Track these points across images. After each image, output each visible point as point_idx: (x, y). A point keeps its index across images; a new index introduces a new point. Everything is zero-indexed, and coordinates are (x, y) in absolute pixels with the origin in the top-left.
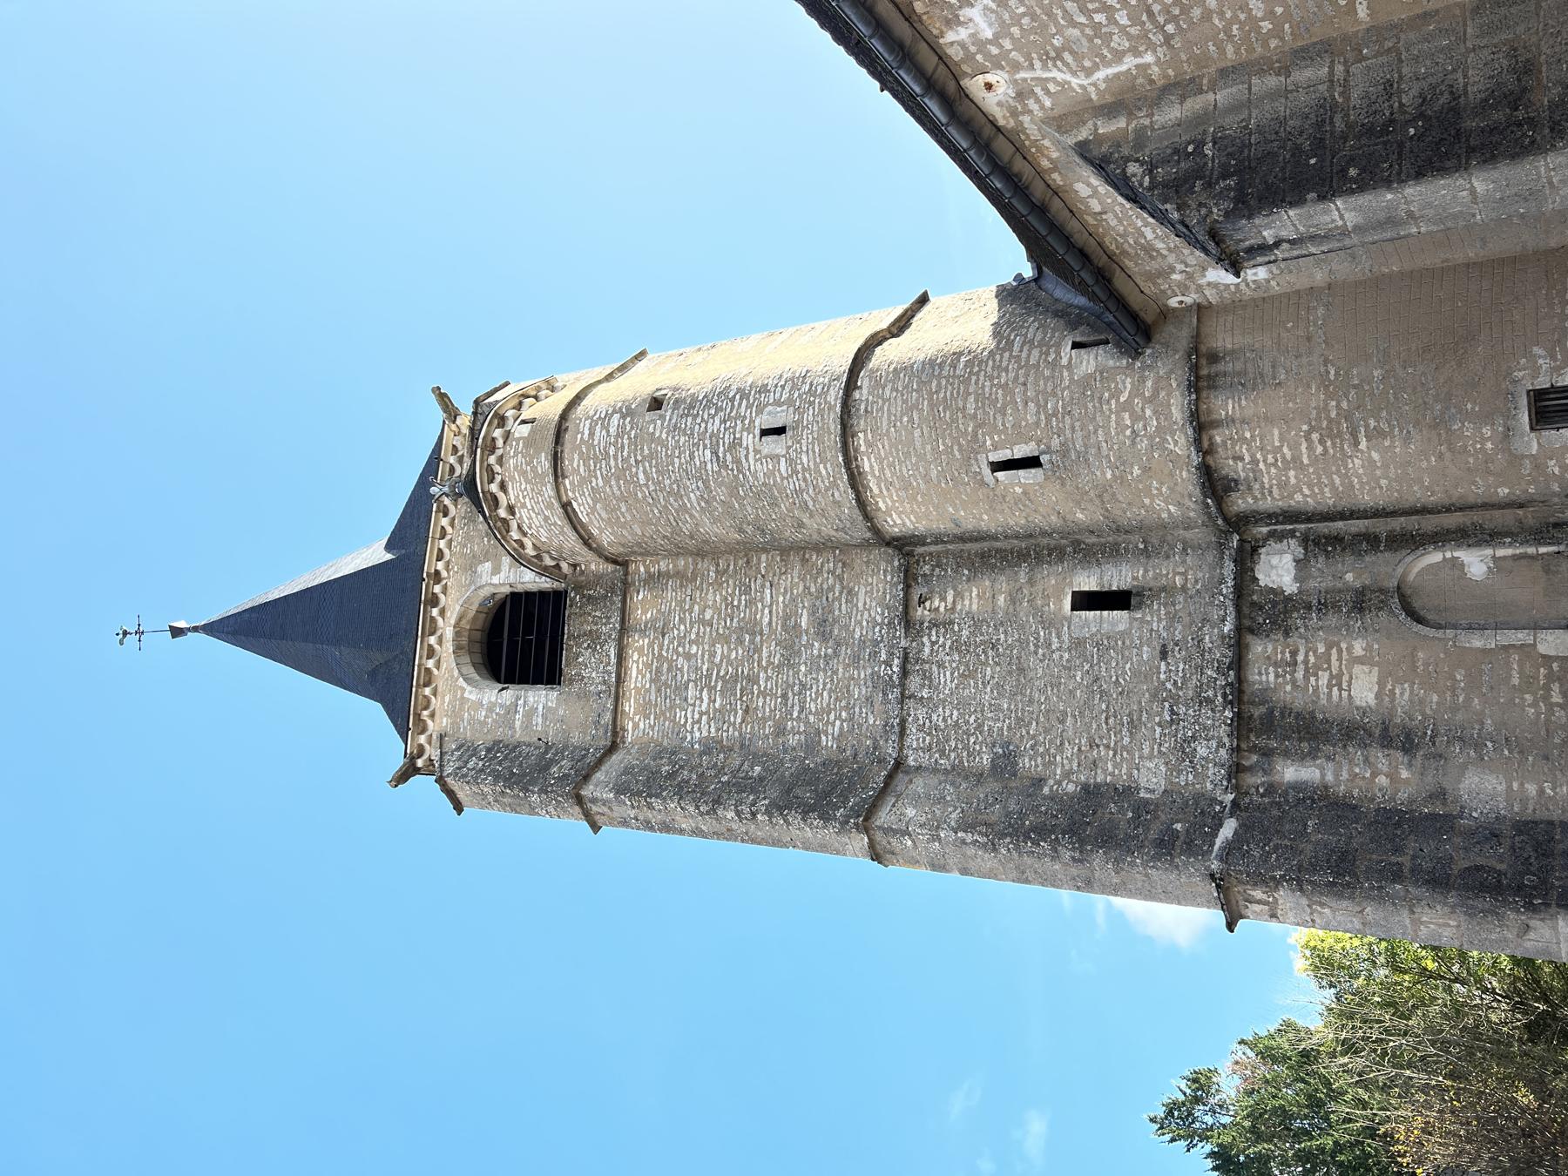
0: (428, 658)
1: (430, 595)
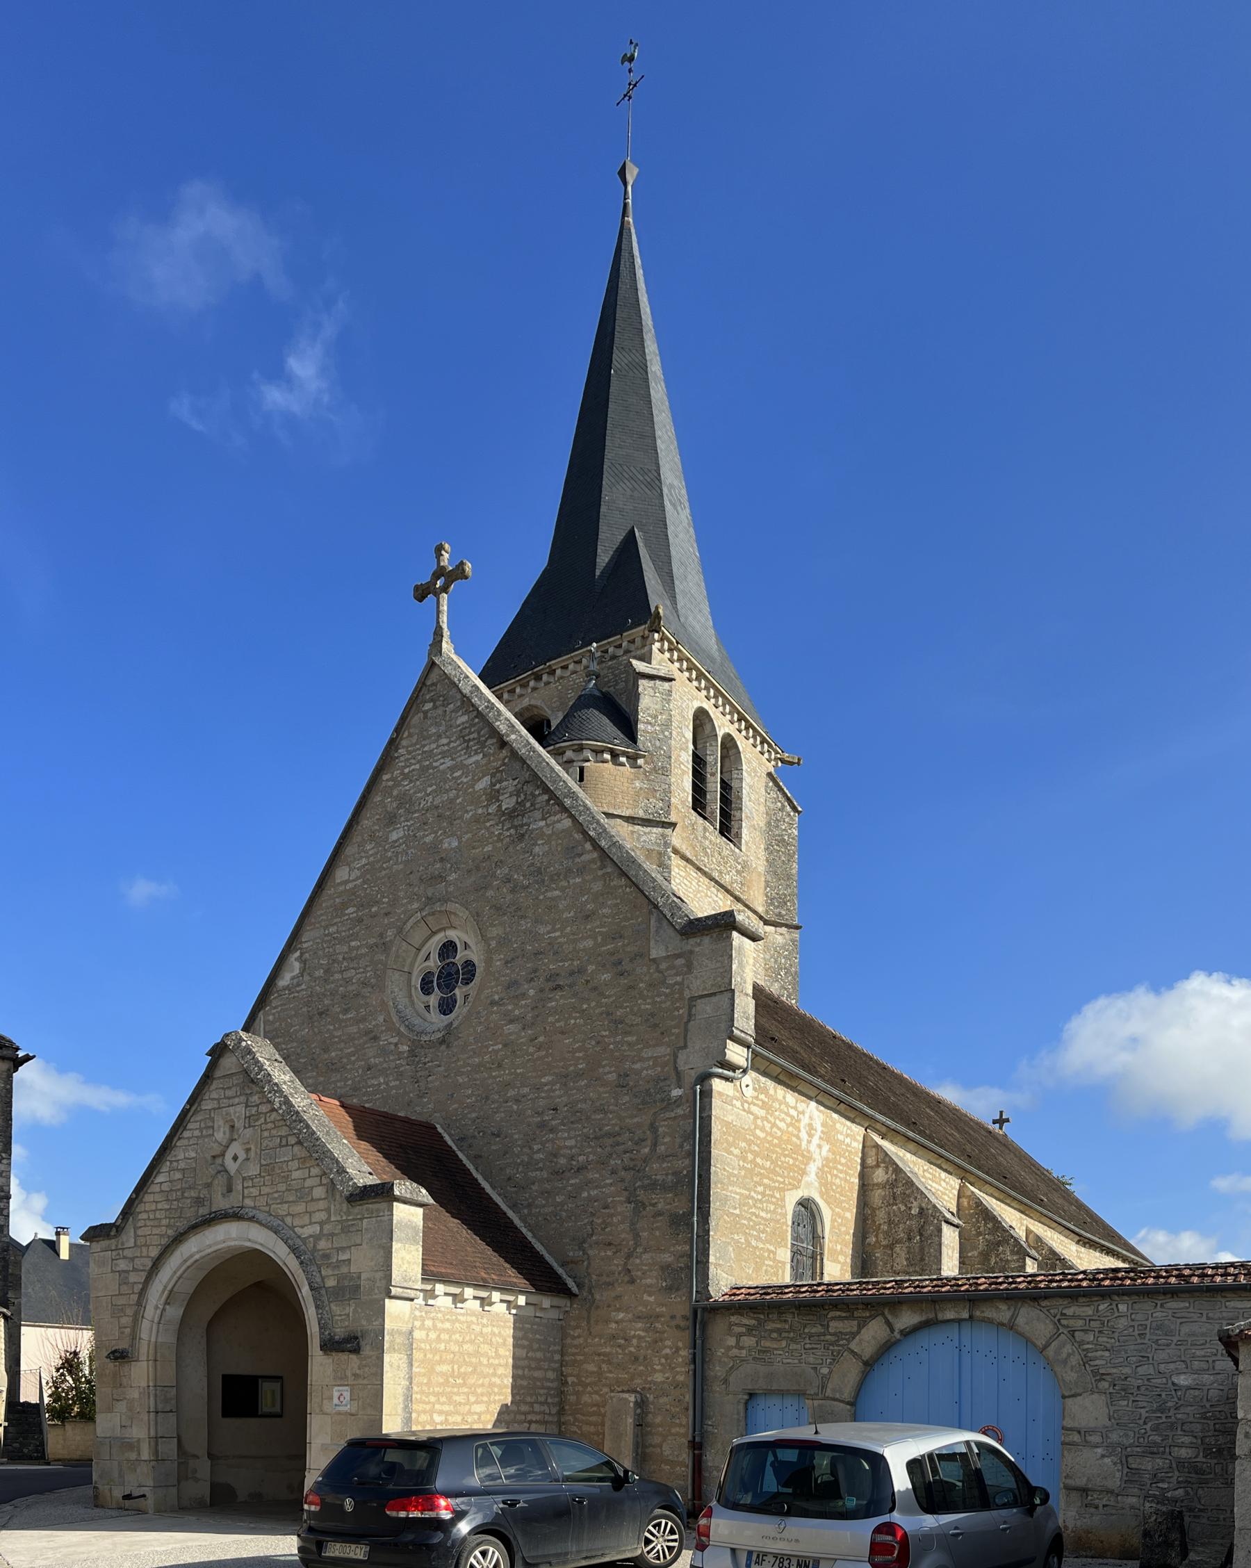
0: (509, 692)
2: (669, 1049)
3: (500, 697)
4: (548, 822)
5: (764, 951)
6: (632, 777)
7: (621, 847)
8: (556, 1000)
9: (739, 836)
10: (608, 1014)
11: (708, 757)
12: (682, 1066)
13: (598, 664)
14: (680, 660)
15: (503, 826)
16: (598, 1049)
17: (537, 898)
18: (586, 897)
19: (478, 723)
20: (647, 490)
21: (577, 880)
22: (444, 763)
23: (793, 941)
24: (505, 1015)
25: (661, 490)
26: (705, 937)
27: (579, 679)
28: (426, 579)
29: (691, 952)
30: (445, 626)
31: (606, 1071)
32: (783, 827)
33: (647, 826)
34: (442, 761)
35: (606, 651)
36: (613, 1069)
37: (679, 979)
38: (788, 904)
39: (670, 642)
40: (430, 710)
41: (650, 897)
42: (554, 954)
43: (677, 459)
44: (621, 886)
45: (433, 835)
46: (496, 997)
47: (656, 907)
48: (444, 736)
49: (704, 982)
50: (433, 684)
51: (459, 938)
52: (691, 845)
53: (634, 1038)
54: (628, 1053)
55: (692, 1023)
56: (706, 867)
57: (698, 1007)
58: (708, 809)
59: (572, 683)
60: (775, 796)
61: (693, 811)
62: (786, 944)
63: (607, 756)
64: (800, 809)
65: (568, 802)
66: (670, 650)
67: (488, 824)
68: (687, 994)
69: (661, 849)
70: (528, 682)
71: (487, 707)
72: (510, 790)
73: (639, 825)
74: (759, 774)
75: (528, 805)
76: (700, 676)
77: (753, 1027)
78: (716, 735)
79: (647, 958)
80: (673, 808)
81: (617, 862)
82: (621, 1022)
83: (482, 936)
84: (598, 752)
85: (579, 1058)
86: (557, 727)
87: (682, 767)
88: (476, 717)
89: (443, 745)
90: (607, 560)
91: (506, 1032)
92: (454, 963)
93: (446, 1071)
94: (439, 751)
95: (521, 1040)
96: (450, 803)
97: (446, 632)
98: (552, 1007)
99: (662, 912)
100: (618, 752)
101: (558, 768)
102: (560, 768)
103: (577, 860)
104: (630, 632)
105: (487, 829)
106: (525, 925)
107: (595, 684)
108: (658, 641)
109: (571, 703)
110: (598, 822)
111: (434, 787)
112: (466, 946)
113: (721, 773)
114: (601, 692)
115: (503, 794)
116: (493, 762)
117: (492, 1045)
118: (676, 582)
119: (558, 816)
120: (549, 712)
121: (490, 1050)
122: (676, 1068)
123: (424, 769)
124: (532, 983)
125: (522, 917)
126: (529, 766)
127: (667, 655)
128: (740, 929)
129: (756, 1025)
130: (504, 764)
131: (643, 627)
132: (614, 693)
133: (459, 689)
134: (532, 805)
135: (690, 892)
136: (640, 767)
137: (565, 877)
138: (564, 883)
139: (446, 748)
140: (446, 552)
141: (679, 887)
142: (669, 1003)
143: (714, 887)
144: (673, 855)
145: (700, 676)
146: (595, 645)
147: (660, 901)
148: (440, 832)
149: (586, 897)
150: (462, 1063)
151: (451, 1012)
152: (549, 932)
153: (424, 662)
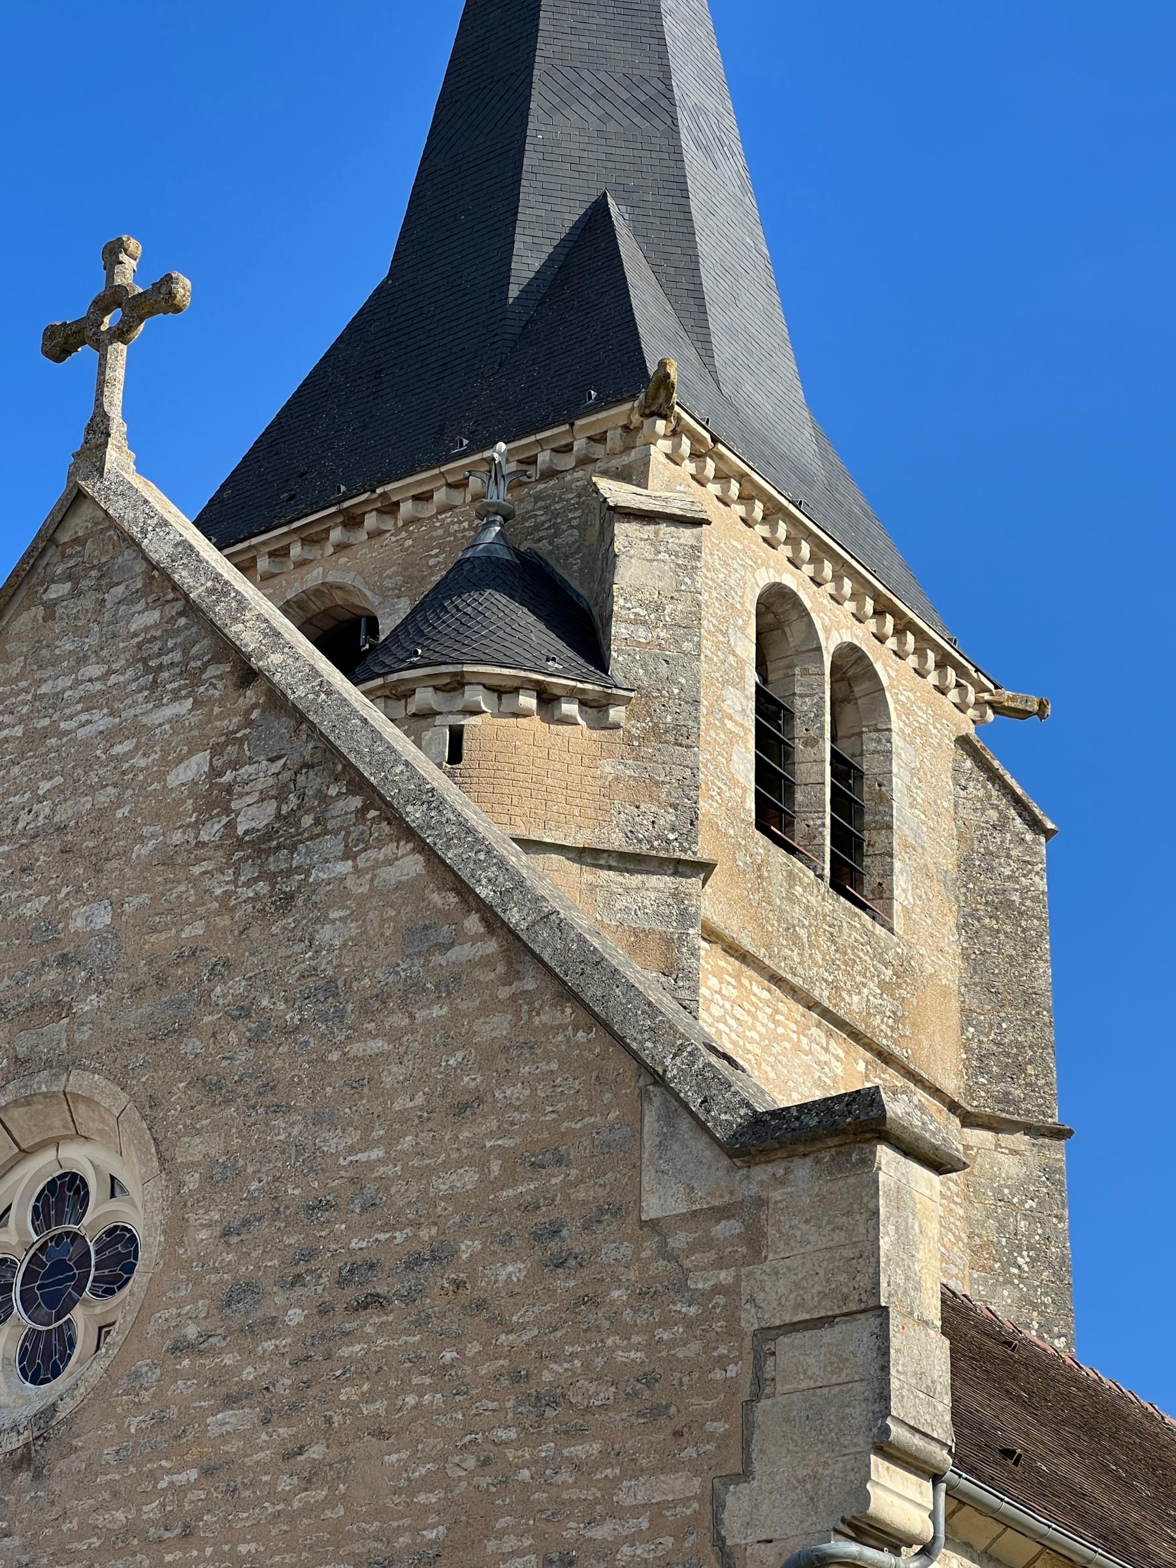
0: (271, 554)
1: (359, 512)
2: (697, 1482)
3: (246, 567)
4: (361, 865)
5: (966, 1198)
6: (594, 749)
7: (562, 926)
8: (369, 1340)
9: (884, 893)
10: (517, 1378)
11: (798, 701)
12: (735, 1534)
13: (510, 489)
14: (721, 477)
15: (237, 874)
16: (483, 1482)
17: (322, 1059)
18: (460, 1055)
19: (186, 627)
20: (637, 119)
21: (436, 1011)
22: (89, 722)
23: (1049, 1171)
24: (213, 1383)
25: (674, 120)
26: (797, 1161)
27: (459, 524)
28: (75, 311)
29: (760, 1202)
30: (115, 412)
31: (507, 1549)
32: (1008, 873)
33: (631, 872)
34: (84, 717)
35: (532, 461)
36: (527, 1543)
37: (725, 1276)
38: (1030, 1070)
39: (695, 438)
40: (62, 599)
41: (643, 1055)
42: (364, 1209)
43: (714, 55)
44: (562, 1028)
45: (45, 899)
46: (191, 1331)
47: (659, 1080)
48: (93, 659)
49: (797, 1285)
50: (75, 541)
51: (95, 1167)
52: (754, 918)
53: (596, 1447)
54: (574, 1494)
55: (765, 1404)
56: (795, 974)
57: (783, 1360)
58: (800, 827)
59: (440, 532)
60: (981, 793)
61: (758, 834)
62: (1029, 1179)
63: (528, 701)
64: (1050, 825)
65: (414, 814)
66: (695, 455)
67: (197, 870)
68: (749, 1320)
69: (672, 929)
70: (327, 531)
71: (211, 591)
72: (260, 787)
73: (610, 868)
74: (935, 742)
75: (307, 821)
76: (773, 513)
77: (948, 1418)
78: (819, 649)
79: (631, 1220)
80: (702, 826)
81: (552, 964)
82: (553, 1403)
83: (162, 1159)
84: (501, 691)
85: (427, 1509)
86: (394, 633)
87: (729, 724)
88: (180, 614)
89: (90, 680)
90: (537, 265)
91: (214, 1431)
92: (75, 1236)
93: (25, 1548)
94: (77, 694)
95: (260, 1456)
96: (97, 818)
97: (118, 428)
98: (351, 1359)
99: (675, 1095)
100: (557, 692)
101: (392, 733)
102: (397, 731)
103: (437, 959)
104: (593, 418)
105: (194, 881)
106: (283, 1129)
107: (499, 534)
108: (665, 437)
109: (436, 578)
110: (502, 864)
111: (59, 780)
112: (114, 1187)
113: (834, 739)
114: (517, 552)
115: (241, 795)
116: (221, 717)
117: (169, 1472)
118: (713, 310)
119: (389, 849)
120: (376, 600)
121: (162, 1485)
122: (719, 1542)
123: (34, 738)
124: (299, 1290)
125: (277, 1109)
126: (313, 726)
127: (689, 467)
128: (898, 1138)
129: (954, 1413)
130: (249, 723)
131: (627, 406)
132: (551, 553)
133: (142, 551)
134: (317, 821)
135: (752, 1041)
136: (617, 727)
137: (404, 1003)
138: (400, 1020)
139: (98, 686)
140: (131, 256)
141: (721, 1026)
142: (695, 1346)
143: (818, 1025)
144: (704, 944)
145: (773, 513)
146: (502, 446)
147: (672, 1067)
148: (65, 890)
149: (460, 1055)
150: (74, 1525)
151: (56, 1373)
152: (352, 1150)
153: (57, 490)
